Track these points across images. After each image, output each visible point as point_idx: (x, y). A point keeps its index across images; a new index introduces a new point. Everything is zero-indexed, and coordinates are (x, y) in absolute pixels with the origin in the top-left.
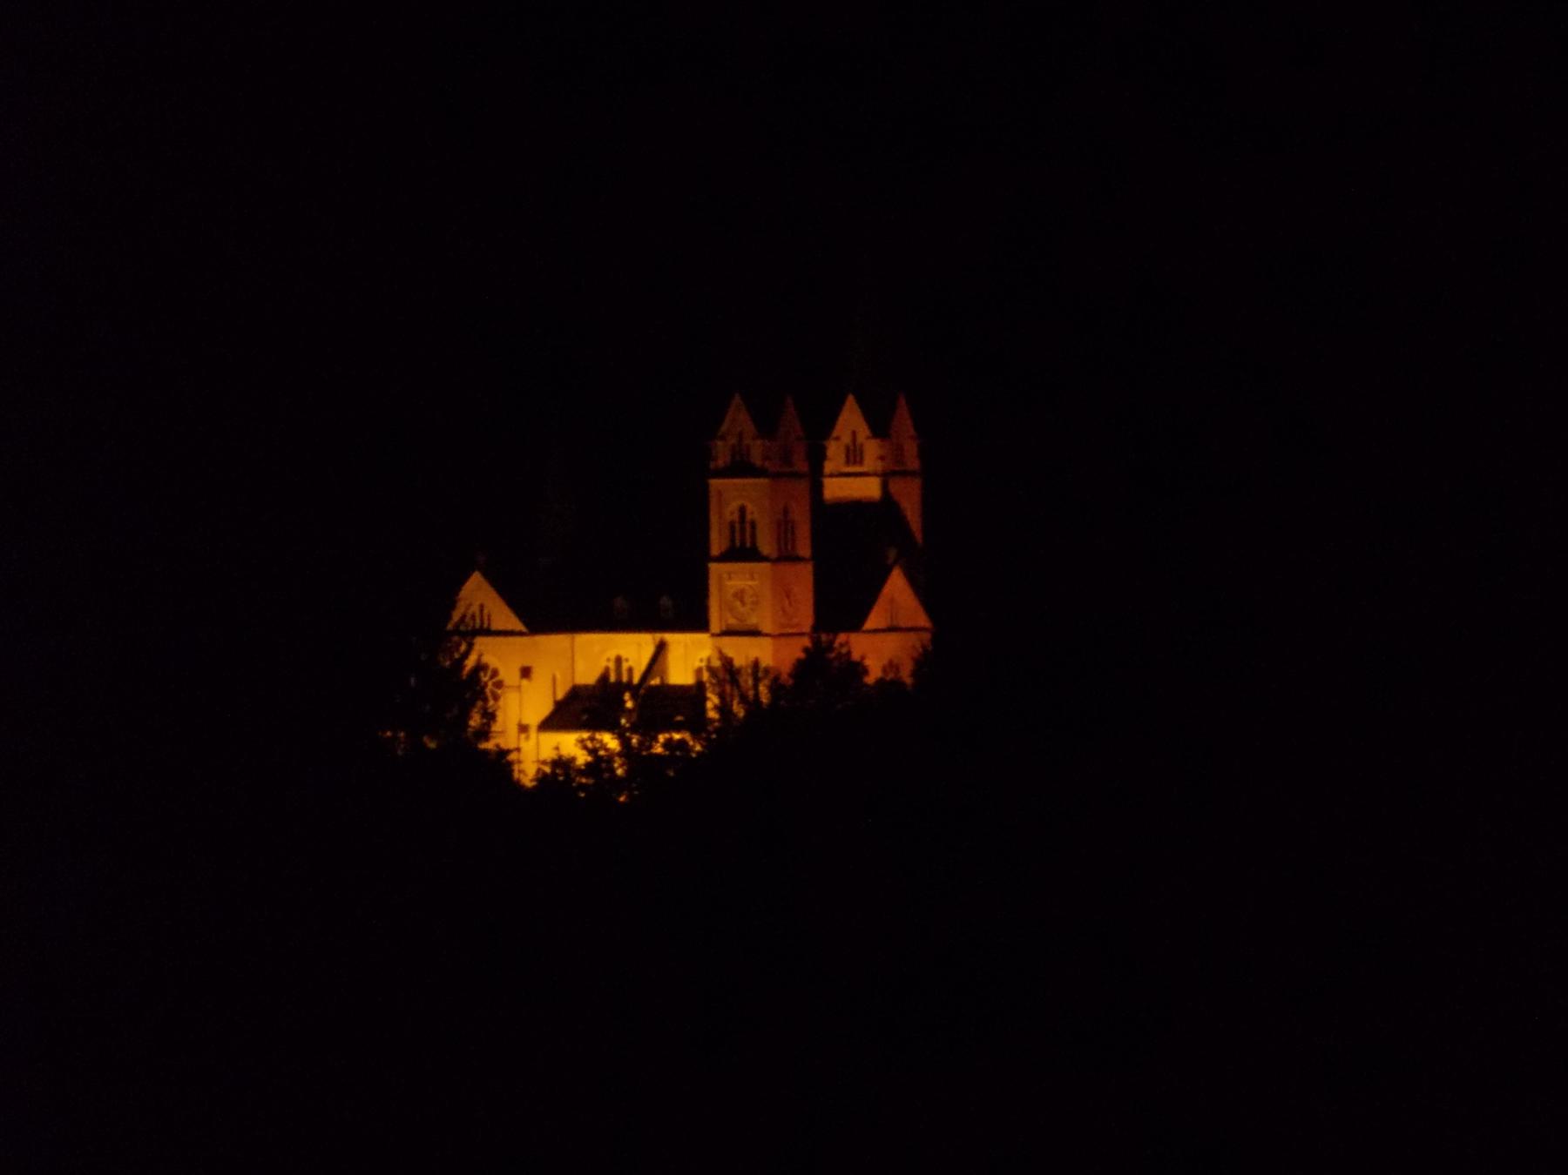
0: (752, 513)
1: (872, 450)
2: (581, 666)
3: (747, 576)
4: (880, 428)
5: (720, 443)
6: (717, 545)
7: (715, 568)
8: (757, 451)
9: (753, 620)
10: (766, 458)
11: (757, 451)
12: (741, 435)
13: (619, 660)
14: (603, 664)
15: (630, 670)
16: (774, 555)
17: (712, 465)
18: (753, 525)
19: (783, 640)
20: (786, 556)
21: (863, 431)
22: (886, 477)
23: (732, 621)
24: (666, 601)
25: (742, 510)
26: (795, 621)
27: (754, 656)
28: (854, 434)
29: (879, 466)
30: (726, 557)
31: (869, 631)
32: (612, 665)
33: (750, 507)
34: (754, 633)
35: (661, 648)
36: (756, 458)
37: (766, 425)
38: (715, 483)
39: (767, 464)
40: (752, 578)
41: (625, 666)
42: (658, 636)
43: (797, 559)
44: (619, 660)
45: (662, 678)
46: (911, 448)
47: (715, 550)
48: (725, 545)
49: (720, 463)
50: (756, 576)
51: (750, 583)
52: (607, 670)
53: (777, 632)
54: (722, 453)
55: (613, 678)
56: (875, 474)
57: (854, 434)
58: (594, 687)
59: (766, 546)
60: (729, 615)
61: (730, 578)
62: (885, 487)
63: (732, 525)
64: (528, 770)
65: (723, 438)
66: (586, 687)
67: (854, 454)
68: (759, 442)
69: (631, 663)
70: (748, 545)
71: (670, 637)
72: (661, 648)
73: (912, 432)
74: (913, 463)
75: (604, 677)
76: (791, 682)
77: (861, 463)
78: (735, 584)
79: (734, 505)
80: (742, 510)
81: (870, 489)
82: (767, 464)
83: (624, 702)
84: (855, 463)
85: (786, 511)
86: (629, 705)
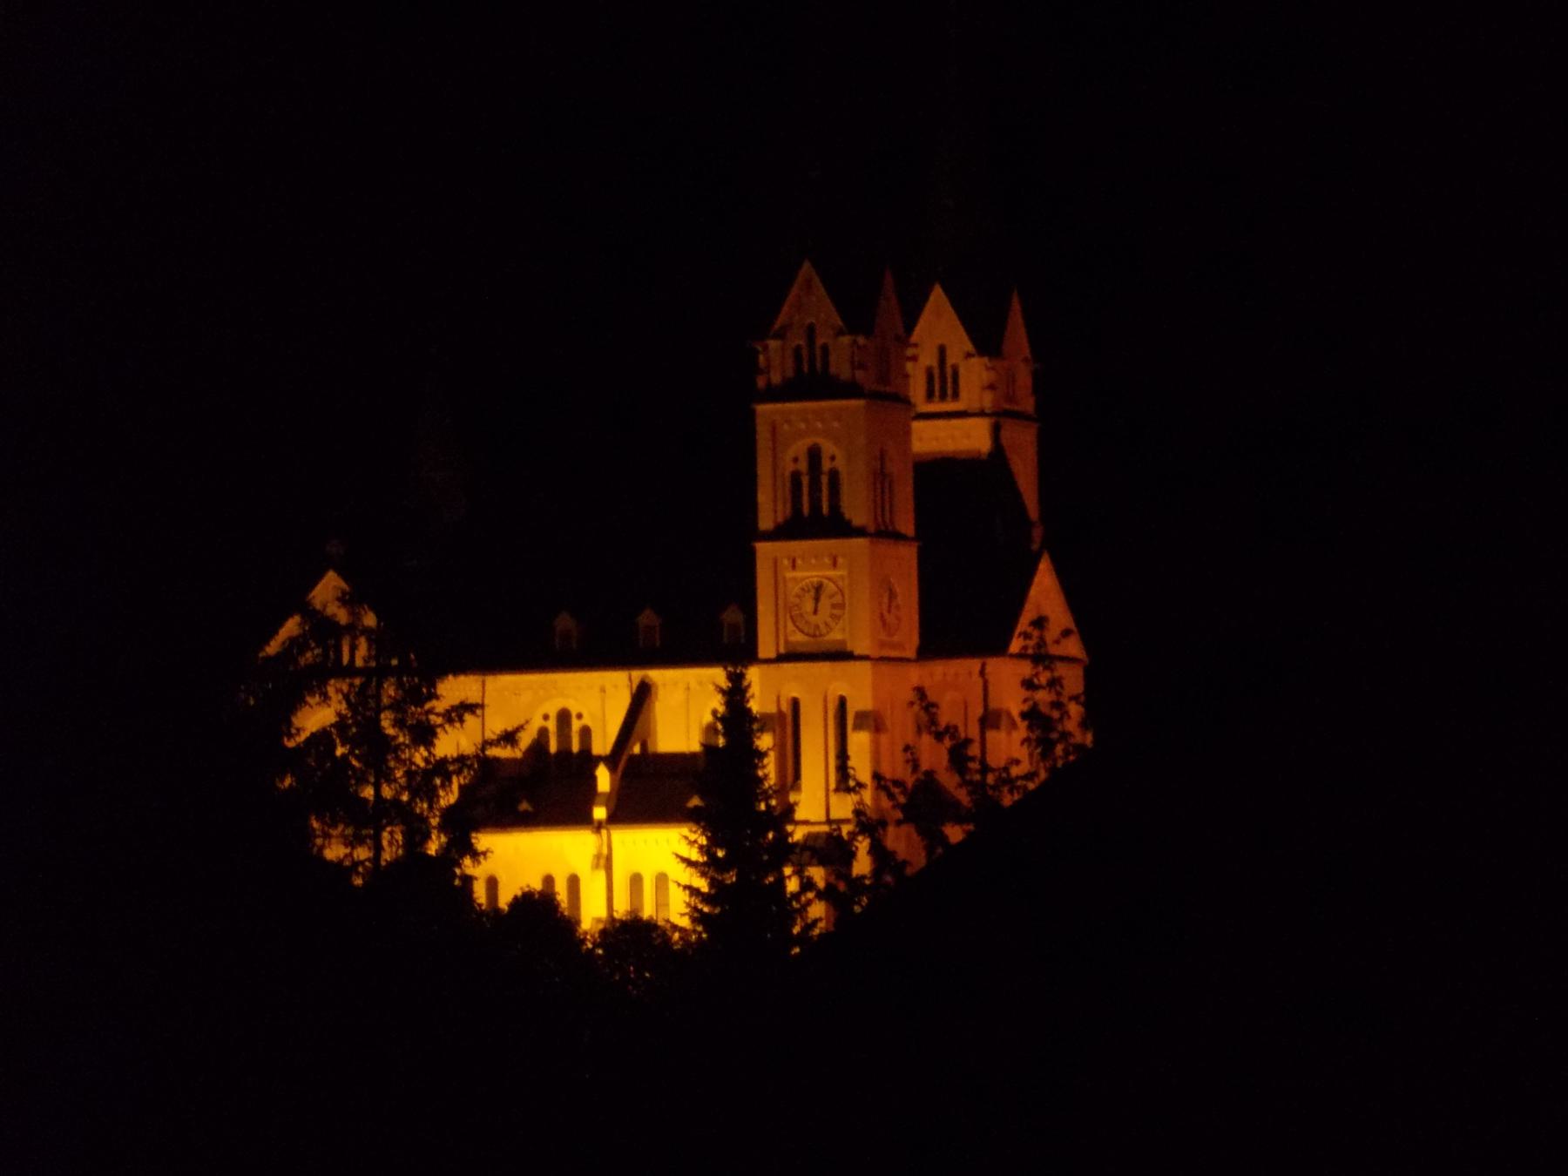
0: (833, 458)
1: (975, 375)
3: (827, 561)
4: (987, 342)
5: (773, 344)
7: (764, 549)
8: (841, 352)
10: (855, 366)
11: (841, 352)
12: (811, 332)
13: (564, 717)
15: (586, 732)
16: (872, 529)
17: (761, 382)
18: (834, 475)
19: (885, 668)
20: (885, 533)
21: (959, 342)
22: (1000, 417)
23: (798, 637)
24: (647, 618)
25: (814, 454)
26: (896, 639)
27: (487, 846)
28: (942, 351)
29: (988, 400)
30: (783, 532)
31: (1012, 656)
32: (552, 725)
33: (828, 447)
34: (840, 655)
35: (642, 696)
36: (840, 367)
37: (857, 317)
38: (762, 408)
39: (860, 374)
40: (835, 564)
41: (576, 725)
42: (637, 675)
43: (897, 537)
44: (564, 717)
45: (644, 745)
46: (1024, 377)
47: (766, 522)
48: (784, 511)
49: (776, 378)
50: (840, 560)
51: (832, 573)
53: (875, 653)
54: (775, 359)
55: (553, 747)
56: (981, 414)
57: (942, 351)
59: (856, 509)
61: (794, 567)
62: (996, 431)
65: (780, 335)
67: (943, 382)
68: (845, 340)
69: (586, 721)
70: (825, 509)
72: (642, 696)
73: (1027, 352)
74: (1028, 405)
76: (506, 908)
77: (956, 396)
78: (808, 575)
79: (800, 447)
80: (814, 454)
81: (972, 437)
82: (860, 374)
84: (943, 397)
85: (882, 456)
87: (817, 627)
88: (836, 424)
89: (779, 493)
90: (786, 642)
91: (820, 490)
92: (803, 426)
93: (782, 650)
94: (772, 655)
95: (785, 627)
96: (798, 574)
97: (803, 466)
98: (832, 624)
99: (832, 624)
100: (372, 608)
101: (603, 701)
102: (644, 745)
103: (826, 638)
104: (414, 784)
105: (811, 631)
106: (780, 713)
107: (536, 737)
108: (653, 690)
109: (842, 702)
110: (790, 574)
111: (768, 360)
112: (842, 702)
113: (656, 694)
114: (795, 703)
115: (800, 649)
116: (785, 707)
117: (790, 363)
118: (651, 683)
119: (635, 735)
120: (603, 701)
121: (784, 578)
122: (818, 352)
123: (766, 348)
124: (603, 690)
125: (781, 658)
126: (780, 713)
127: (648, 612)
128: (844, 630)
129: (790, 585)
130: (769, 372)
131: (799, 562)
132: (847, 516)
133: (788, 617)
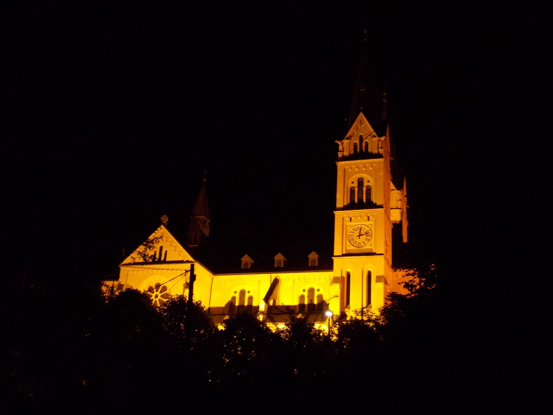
2: (215, 295)
3: (365, 218)
5: (347, 141)
6: (341, 199)
7: (338, 214)
9: (367, 247)
13: (243, 293)
14: (233, 294)
15: (251, 298)
17: (340, 155)
18: (369, 190)
25: (360, 182)
30: (345, 208)
32: (237, 296)
35: (275, 283)
36: (373, 149)
38: (340, 164)
41: (247, 295)
42: (274, 276)
45: (274, 301)
48: (347, 202)
49: (346, 153)
50: (371, 218)
52: (234, 298)
55: (237, 304)
58: (224, 307)
60: (348, 243)
63: (352, 191)
64: (220, 329)
66: (134, 290)
69: (251, 294)
71: (282, 276)
72: (275, 283)
75: (231, 304)
80: (360, 182)
83: (253, 340)
86: (124, 251)
87: (360, 243)
88: (371, 168)
89: (346, 194)
90: (346, 250)
91: (354, 197)
92: (357, 170)
93: (344, 253)
94: (357, 246)
95: (346, 244)
96: (352, 224)
97: (355, 185)
98: (366, 242)
99: (366, 242)
100: (154, 308)
101: (259, 286)
102: (274, 301)
103: (363, 248)
104: (183, 326)
105: (357, 246)
106: (342, 277)
107: (230, 299)
108: (280, 282)
109: (369, 274)
110: (349, 224)
111: (343, 148)
112: (369, 274)
113: (281, 283)
114: (348, 275)
115: (352, 252)
116: (345, 275)
117: (352, 147)
118: (279, 279)
119: (272, 297)
120: (259, 286)
121: (346, 225)
122: (364, 145)
123: (342, 143)
124: (259, 282)
125: (343, 255)
126: (342, 277)
127: (279, 254)
128: (371, 245)
129: (348, 228)
130: (343, 152)
131: (353, 219)
132: (374, 202)
133: (347, 241)
